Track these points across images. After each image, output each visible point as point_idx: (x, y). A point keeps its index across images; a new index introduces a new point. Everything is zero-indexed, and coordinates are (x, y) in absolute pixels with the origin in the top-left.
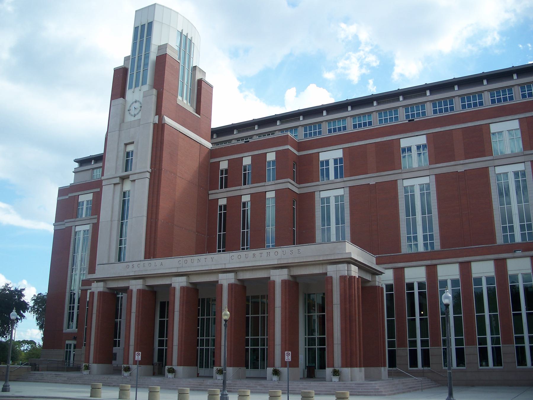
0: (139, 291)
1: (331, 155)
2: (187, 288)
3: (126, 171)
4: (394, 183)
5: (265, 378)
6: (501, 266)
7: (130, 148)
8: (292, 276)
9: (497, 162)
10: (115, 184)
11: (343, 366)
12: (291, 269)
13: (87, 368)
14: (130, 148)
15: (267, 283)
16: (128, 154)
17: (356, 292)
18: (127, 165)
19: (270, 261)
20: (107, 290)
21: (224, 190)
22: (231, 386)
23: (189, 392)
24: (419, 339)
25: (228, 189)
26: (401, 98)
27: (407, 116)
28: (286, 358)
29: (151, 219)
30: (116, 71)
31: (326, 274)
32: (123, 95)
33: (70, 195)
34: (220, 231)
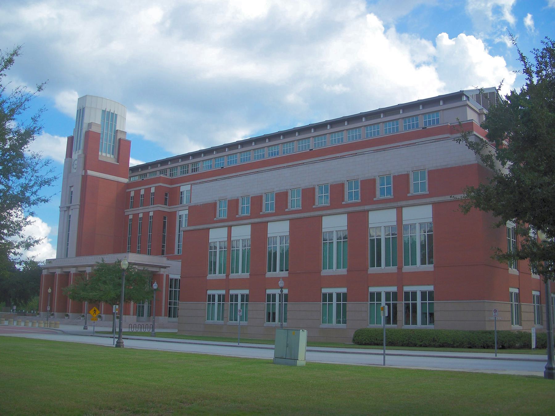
21: (152, 206)
26: (401, 112)
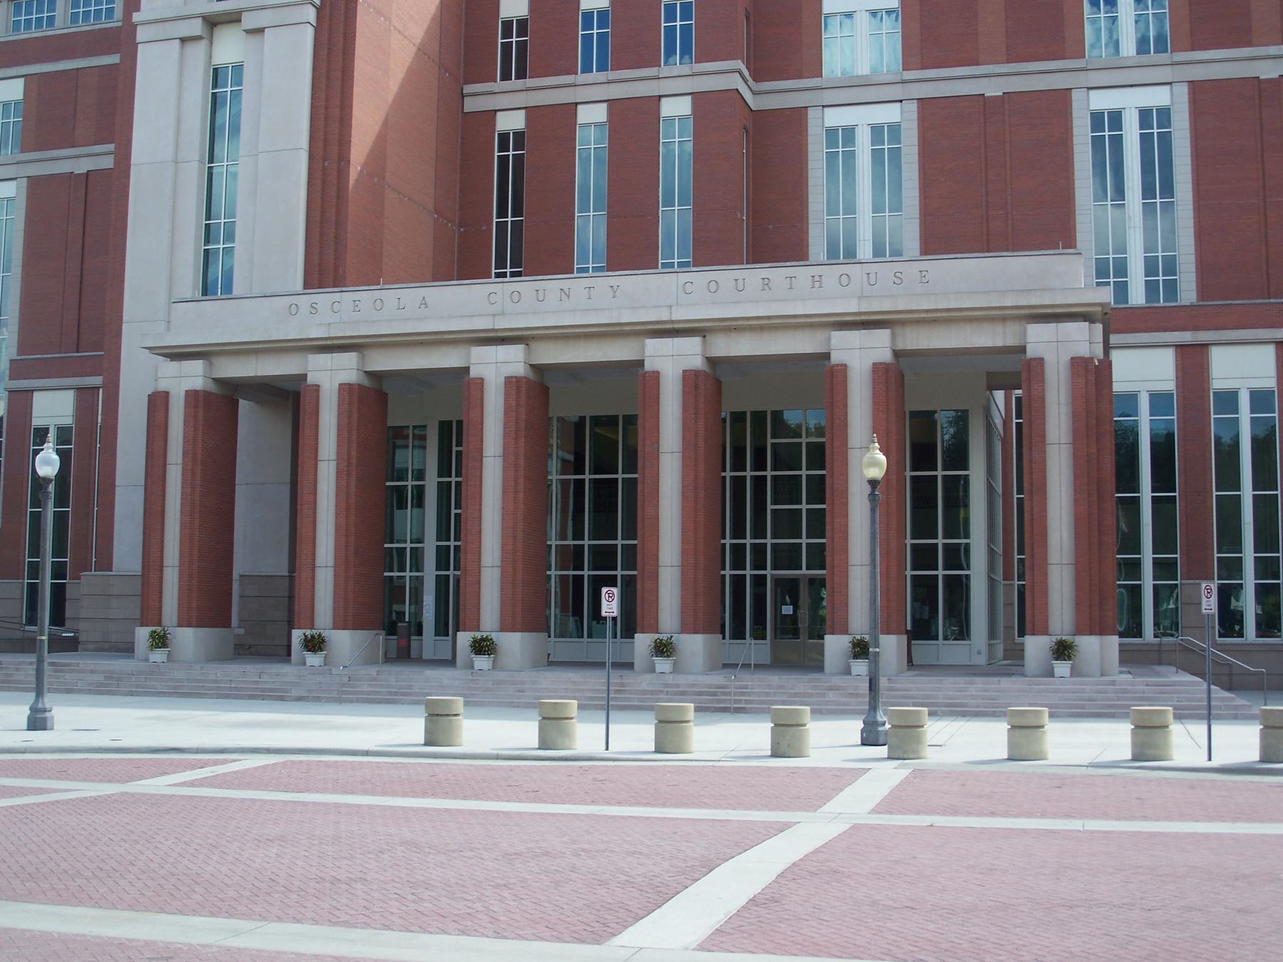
0: (345, 389)
2: (206, 394)
4: (1064, 96)
5: (630, 666)
8: (370, 374)
9: (829, 97)
10: (183, 40)
11: (503, 629)
12: (899, 330)
13: (160, 641)
15: (461, 383)
19: (663, 315)
20: (212, 387)
21: (514, 83)
22: (729, 693)
23: (691, 715)
25: (529, 82)
28: (1204, 606)
29: (325, 159)
34: (502, 212)
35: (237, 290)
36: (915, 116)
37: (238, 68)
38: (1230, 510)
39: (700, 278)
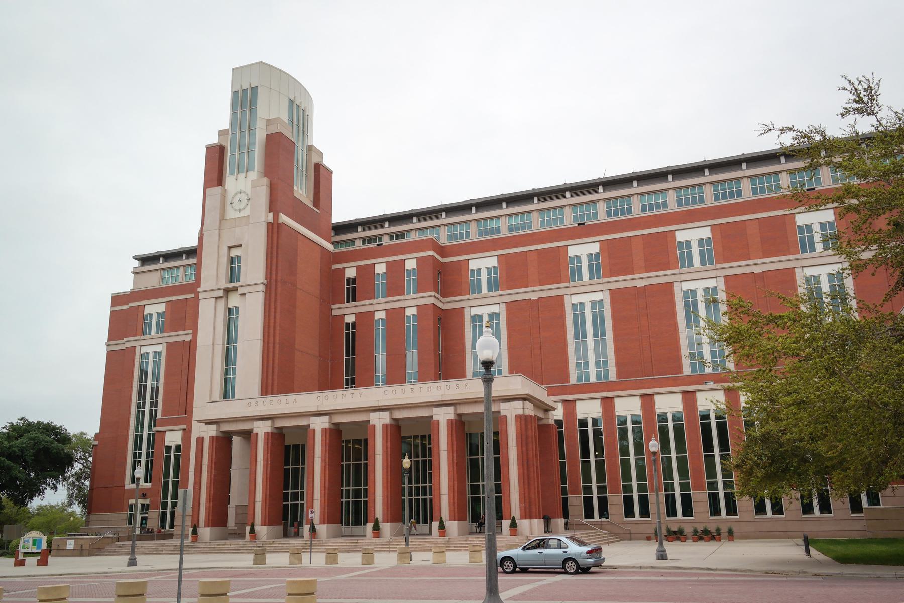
0: (267, 434)
1: (483, 264)
3: (231, 282)
6: (689, 398)
7: (235, 253)
10: (216, 298)
12: (458, 406)
14: (235, 253)
16: (232, 260)
17: (533, 433)
18: (233, 273)
21: (351, 304)
24: (594, 485)
27: (575, 217)
30: (210, 149)
31: (499, 412)
32: (220, 182)
33: (131, 304)
34: (347, 355)
35: (236, 397)
36: (505, 309)
37: (237, 308)
38: (626, 464)
39: (390, 389)
